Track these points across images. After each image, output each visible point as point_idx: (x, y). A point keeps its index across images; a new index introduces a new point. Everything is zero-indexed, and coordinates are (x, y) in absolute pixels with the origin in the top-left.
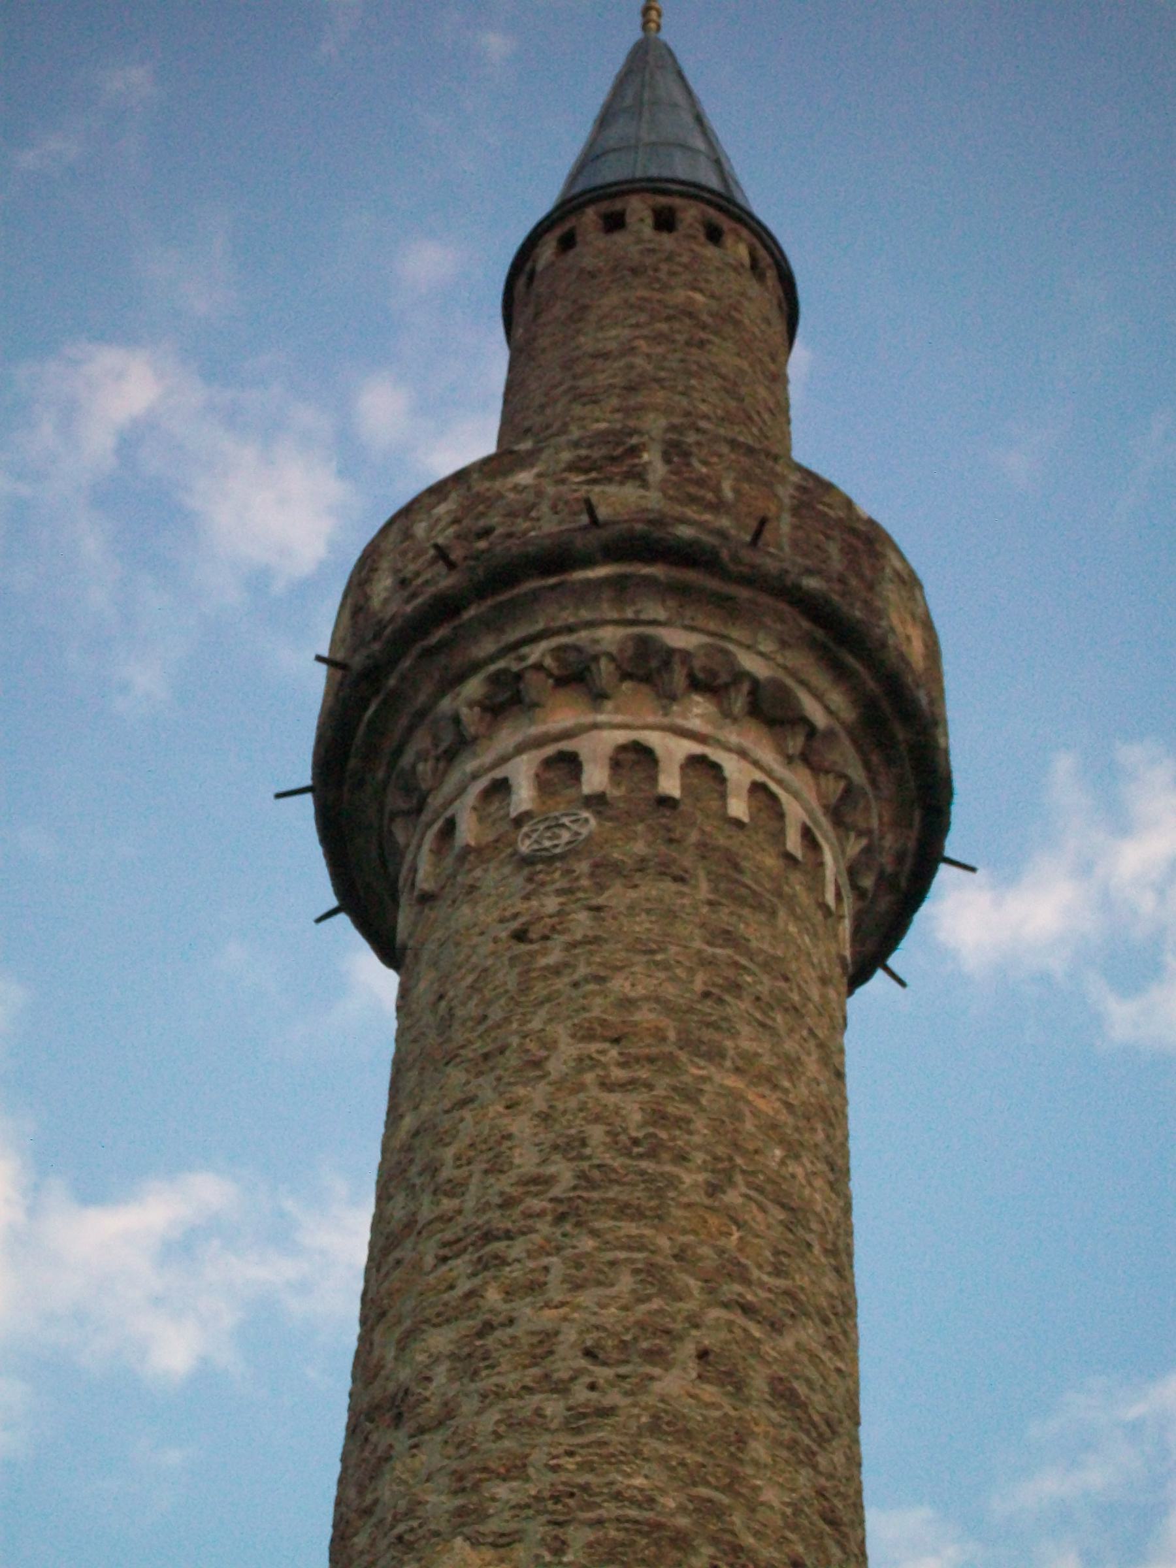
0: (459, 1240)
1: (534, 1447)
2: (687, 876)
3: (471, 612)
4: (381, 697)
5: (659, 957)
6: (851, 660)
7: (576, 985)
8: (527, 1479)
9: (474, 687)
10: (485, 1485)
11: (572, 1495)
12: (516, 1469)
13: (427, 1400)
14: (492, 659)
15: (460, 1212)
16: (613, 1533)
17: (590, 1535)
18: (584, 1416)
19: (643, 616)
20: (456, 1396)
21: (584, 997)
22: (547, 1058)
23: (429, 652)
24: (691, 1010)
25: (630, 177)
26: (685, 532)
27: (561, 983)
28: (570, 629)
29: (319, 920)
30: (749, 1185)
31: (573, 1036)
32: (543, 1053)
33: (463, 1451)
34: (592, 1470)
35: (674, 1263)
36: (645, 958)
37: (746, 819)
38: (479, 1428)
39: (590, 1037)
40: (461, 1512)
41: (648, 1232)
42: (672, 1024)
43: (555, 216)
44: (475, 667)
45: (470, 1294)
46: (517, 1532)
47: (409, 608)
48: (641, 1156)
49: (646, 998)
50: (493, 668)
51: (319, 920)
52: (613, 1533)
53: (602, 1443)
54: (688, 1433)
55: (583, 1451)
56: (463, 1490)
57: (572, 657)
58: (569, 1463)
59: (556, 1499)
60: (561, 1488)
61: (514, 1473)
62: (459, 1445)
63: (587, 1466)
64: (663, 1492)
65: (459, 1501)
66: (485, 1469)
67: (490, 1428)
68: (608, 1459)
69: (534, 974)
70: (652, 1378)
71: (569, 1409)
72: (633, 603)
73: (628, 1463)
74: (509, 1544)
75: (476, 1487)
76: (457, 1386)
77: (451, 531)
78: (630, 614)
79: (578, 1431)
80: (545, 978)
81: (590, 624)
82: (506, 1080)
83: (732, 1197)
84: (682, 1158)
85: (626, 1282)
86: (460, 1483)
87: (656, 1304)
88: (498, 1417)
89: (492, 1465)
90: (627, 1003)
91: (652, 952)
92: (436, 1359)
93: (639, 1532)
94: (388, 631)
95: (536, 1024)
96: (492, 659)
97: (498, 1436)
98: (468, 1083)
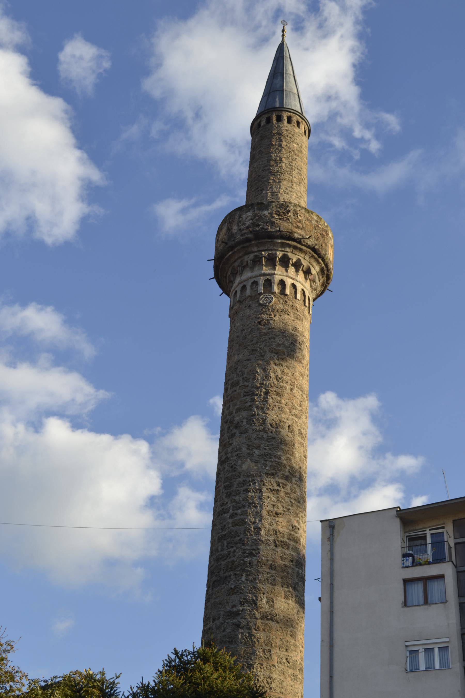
0: (248, 392)
1: (262, 443)
3: (253, 242)
4: (233, 252)
7: (270, 339)
8: (260, 450)
9: (252, 256)
10: (253, 449)
11: (268, 455)
12: (258, 447)
13: (242, 426)
14: (256, 252)
15: (248, 386)
16: (274, 464)
17: (270, 464)
18: (270, 439)
19: (285, 250)
20: (248, 428)
21: (271, 342)
22: (264, 355)
23: (244, 247)
24: (289, 347)
27: (267, 338)
28: (272, 250)
29: (210, 279)
31: (269, 351)
32: (264, 354)
33: (249, 441)
34: (271, 450)
35: (285, 406)
36: (282, 334)
37: (300, 299)
38: (252, 437)
39: (272, 352)
40: (249, 454)
42: (286, 350)
44: (252, 252)
45: (250, 406)
46: (258, 461)
47: (241, 238)
49: (282, 344)
50: (256, 254)
51: (210, 279)
52: (274, 464)
53: (272, 445)
55: (270, 446)
56: (249, 449)
57: (271, 256)
59: (265, 455)
60: (266, 453)
61: (258, 448)
62: (248, 439)
63: (270, 449)
65: (249, 452)
66: (253, 446)
67: (254, 437)
68: (274, 448)
69: (262, 334)
71: (268, 437)
72: (284, 247)
73: (277, 449)
74: (257, 463)
75: (252, 450)
76: (248, 426)
77: (251, 221)
78: (283, 250)
79: (269, 442)
80: (264, 335)
82: (257, 358)
86: (249, 447)
88: (255, 435)
89: (255, 445)
90: (279, 345)
92: (244, 418)
93: (278, 464)
94: (236, 240)
95: (262, 346)
96: (256, 252)
98: (249, 355)
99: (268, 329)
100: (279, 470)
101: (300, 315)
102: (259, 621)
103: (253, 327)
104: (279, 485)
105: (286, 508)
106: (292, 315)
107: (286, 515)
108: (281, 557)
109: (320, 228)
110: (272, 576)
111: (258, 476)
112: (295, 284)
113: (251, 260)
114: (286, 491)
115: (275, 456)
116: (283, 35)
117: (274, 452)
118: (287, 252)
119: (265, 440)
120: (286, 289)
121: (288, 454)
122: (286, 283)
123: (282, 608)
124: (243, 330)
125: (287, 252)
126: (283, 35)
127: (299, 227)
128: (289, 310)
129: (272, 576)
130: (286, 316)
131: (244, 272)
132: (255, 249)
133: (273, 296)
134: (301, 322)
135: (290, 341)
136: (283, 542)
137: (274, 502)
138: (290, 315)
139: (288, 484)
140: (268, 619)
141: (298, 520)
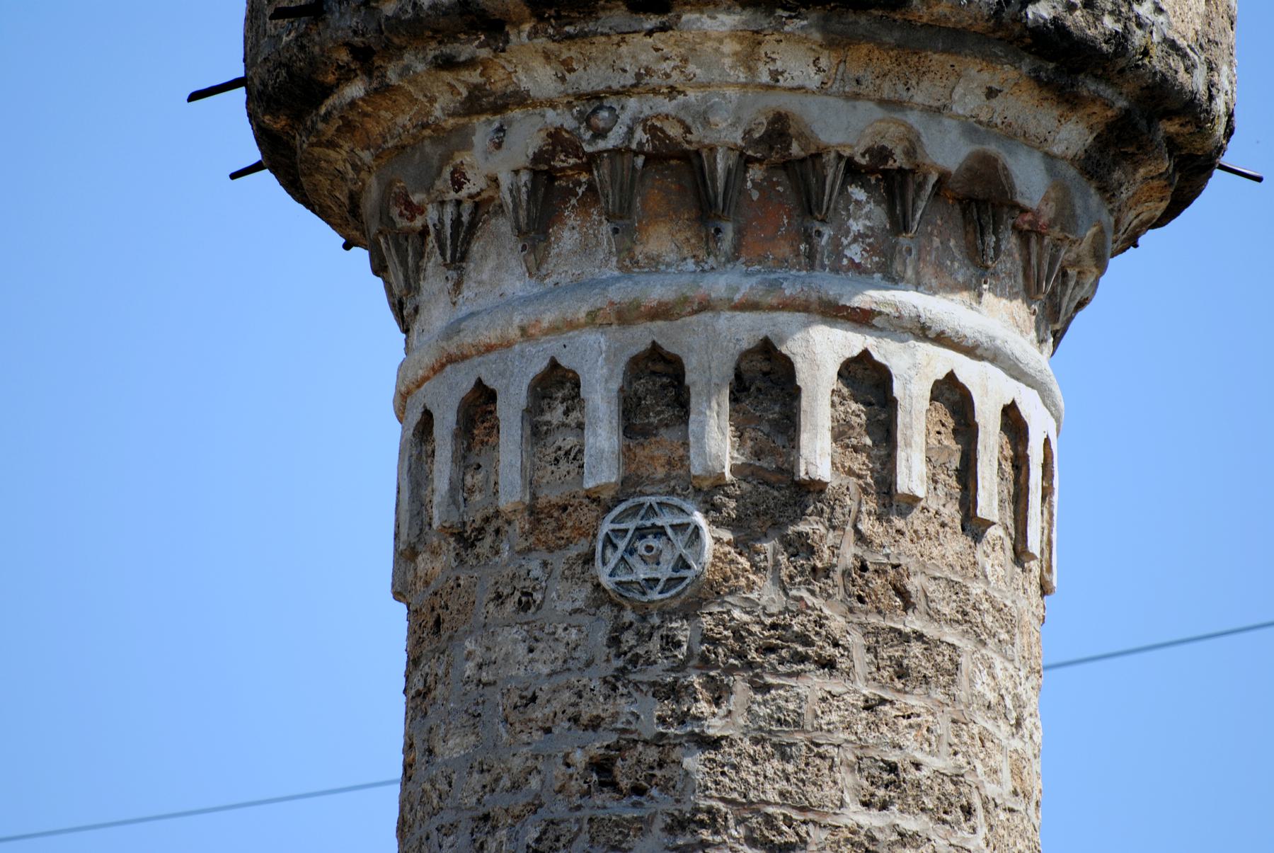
29: (234, 176)
99: (669, 829)
101: (930, 631)
103: (559, 809)
106: (861, 659)
111: (846, 510)
112: (877, 356)
120: (804, 438)
122: (802, 378)
124: (486, 818)
128: (837, 623)
130: (814, 684)
131: (476, 247)
133: (699, 518)
134: (938, 694)
138: (843, 664)
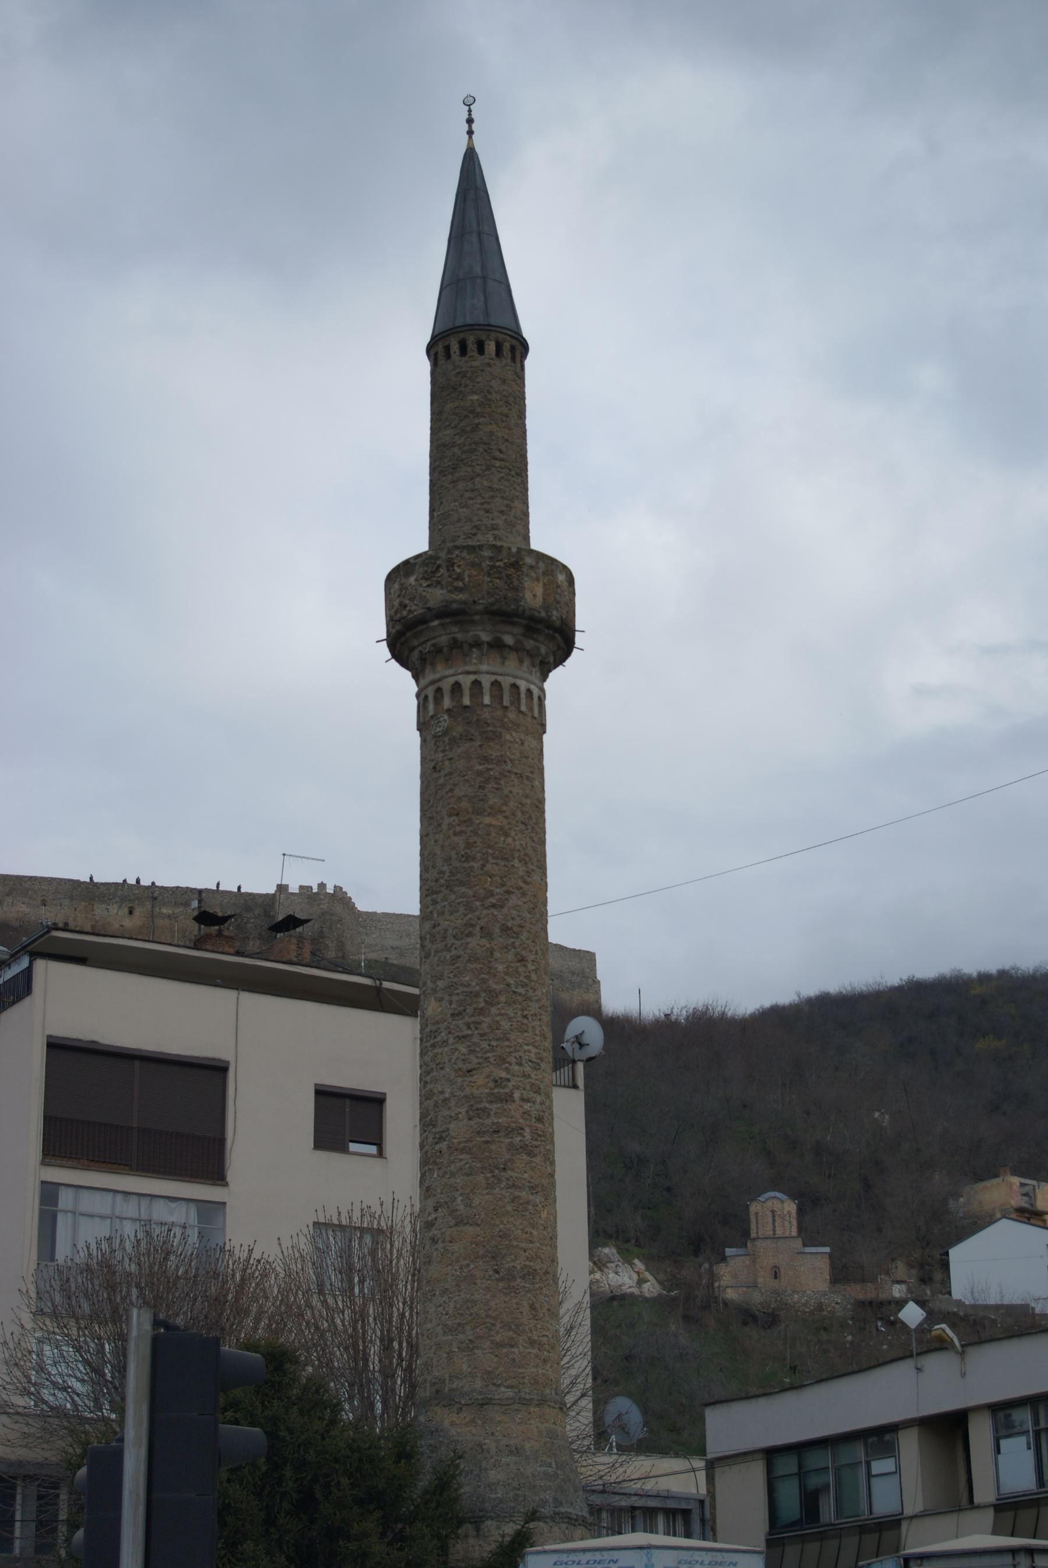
2: (473, 737)
5: (466, 778)
6: (515, 620)
14: (418, 646)
25: (452, 327)
26: (455, 606)
28: (434, 638)
30: (494, 858)
41: (466, 890)
43: (432, 343)
48: (464, 862)
49: (464, 796)
53: (458, 968)
54: (478, 959)
58: (451, 975)
63: (455, 976)
64: (472, 980)
70: (468, 943)
78: (448, 632)
79: (453, 964)
81: (439, 636)
83: (489, 867)
84: (474, 859)
85: (462, 909)
87: (470, 916)
91: (464, 776)
97: (438, 965)
100: (468, 1005)
102: (35, 1349)
104: (469, 1028)
105: (482, 1057)
107: (484, 1067)
108: (478, 1133)
109: (499, 567)
110: (467, 1163)
112: (479, 680)
113: (417, 660)
114: (482, 1032)
115: (462, 985)
116: (470, 133)
117: (461, 978)
118: (455, 633)
119: (448, 963)
121: (483, 973)
123: (483, 1204)
125: (455, 633)
126: (470, 133)
127: (458, 587)
129: (467, 1163)
132: (415, 643)
135: (477, 786)
136: (481, 1109)
137: (465, 1055)
139: (484, 1019)
140: (465, 1224)
141: (506, 1068)
